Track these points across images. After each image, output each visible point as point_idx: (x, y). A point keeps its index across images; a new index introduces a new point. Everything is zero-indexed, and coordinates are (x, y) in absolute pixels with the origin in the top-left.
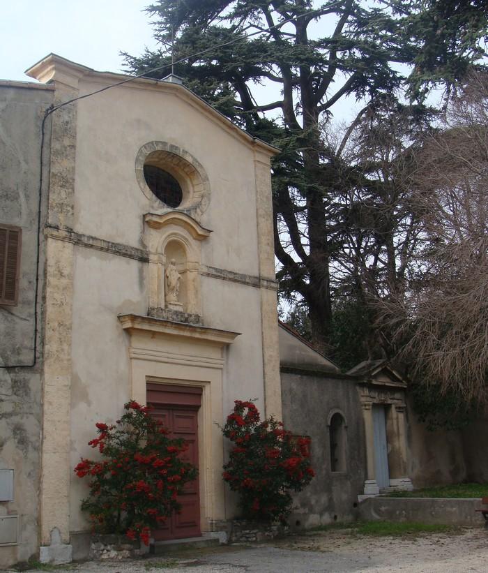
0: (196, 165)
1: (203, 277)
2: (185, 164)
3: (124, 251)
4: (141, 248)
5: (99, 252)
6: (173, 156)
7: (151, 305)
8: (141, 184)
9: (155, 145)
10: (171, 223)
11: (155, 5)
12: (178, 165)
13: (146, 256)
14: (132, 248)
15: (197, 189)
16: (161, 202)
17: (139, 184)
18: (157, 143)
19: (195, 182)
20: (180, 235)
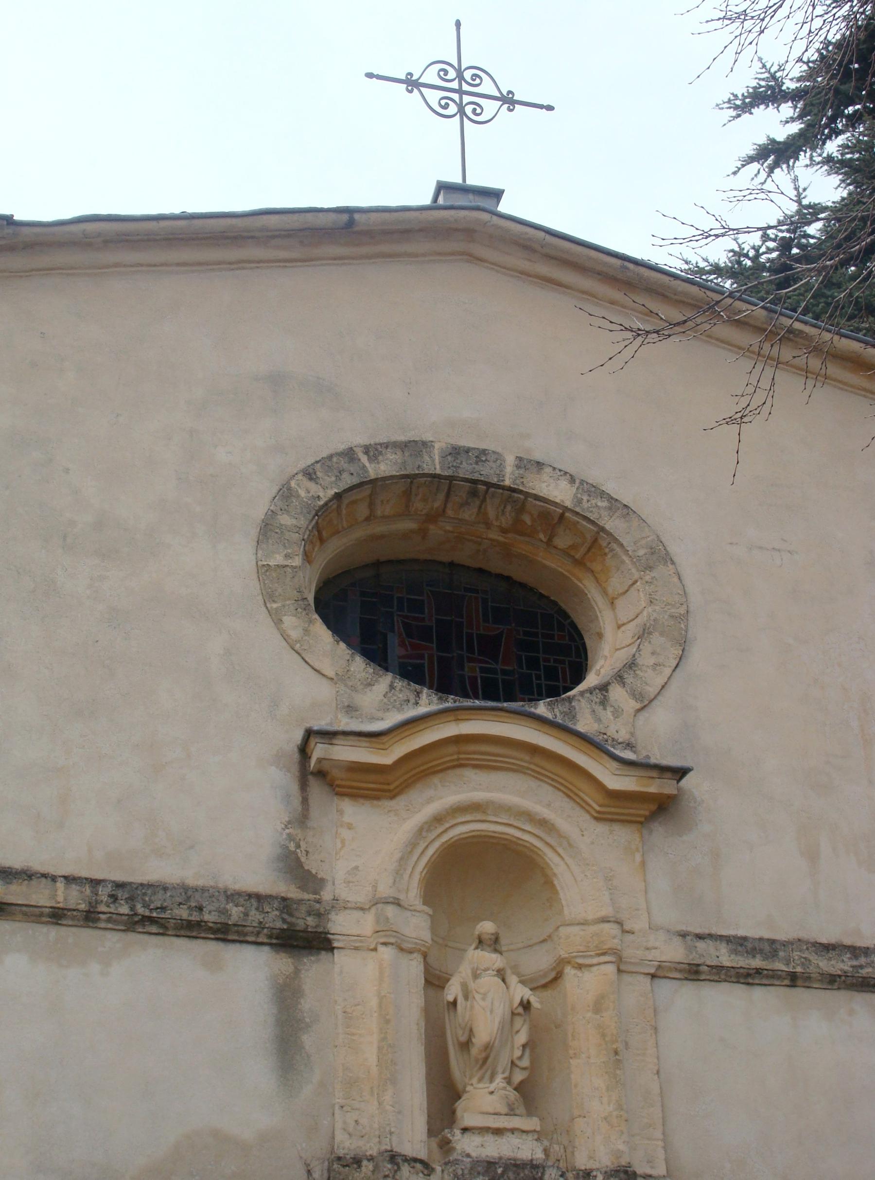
0: (595, 509)
1: (665, 987)
2: (545, 516)
3: (183, 913)
4: (293, 893)
5: (51, 933)
6: (474, 493)
7: (347, 1145)
8: (289, 621)
9: (364, 459)
10: (460, 765)
11: (781, 137)
12: (517, 528)
13: (311, 921)
14: (232, 896)
15: (625, 609)
16: (399, 684)
17: (278, 622)
18: (373, 451)
19: (615, 584)
20: (508, 809)
